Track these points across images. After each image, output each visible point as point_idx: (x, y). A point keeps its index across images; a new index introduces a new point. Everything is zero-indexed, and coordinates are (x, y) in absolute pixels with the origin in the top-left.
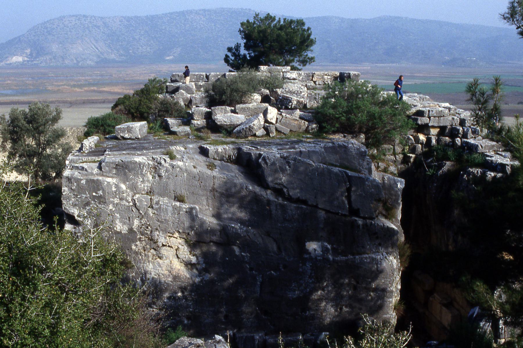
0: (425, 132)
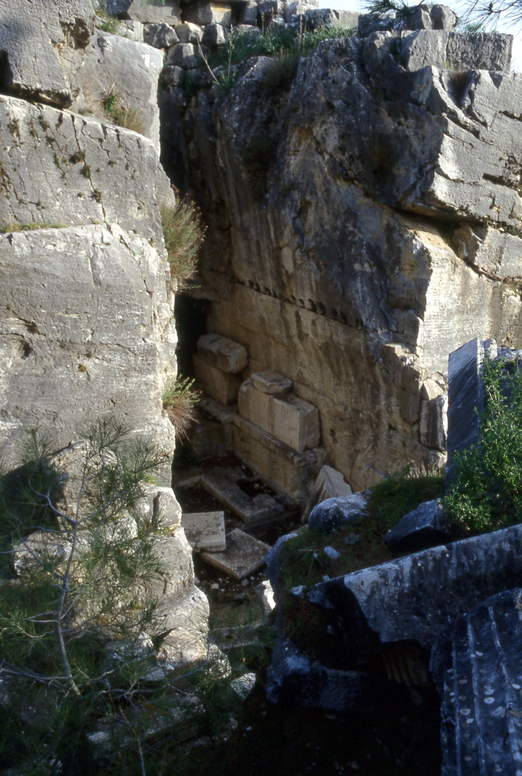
0: (200, 15)
